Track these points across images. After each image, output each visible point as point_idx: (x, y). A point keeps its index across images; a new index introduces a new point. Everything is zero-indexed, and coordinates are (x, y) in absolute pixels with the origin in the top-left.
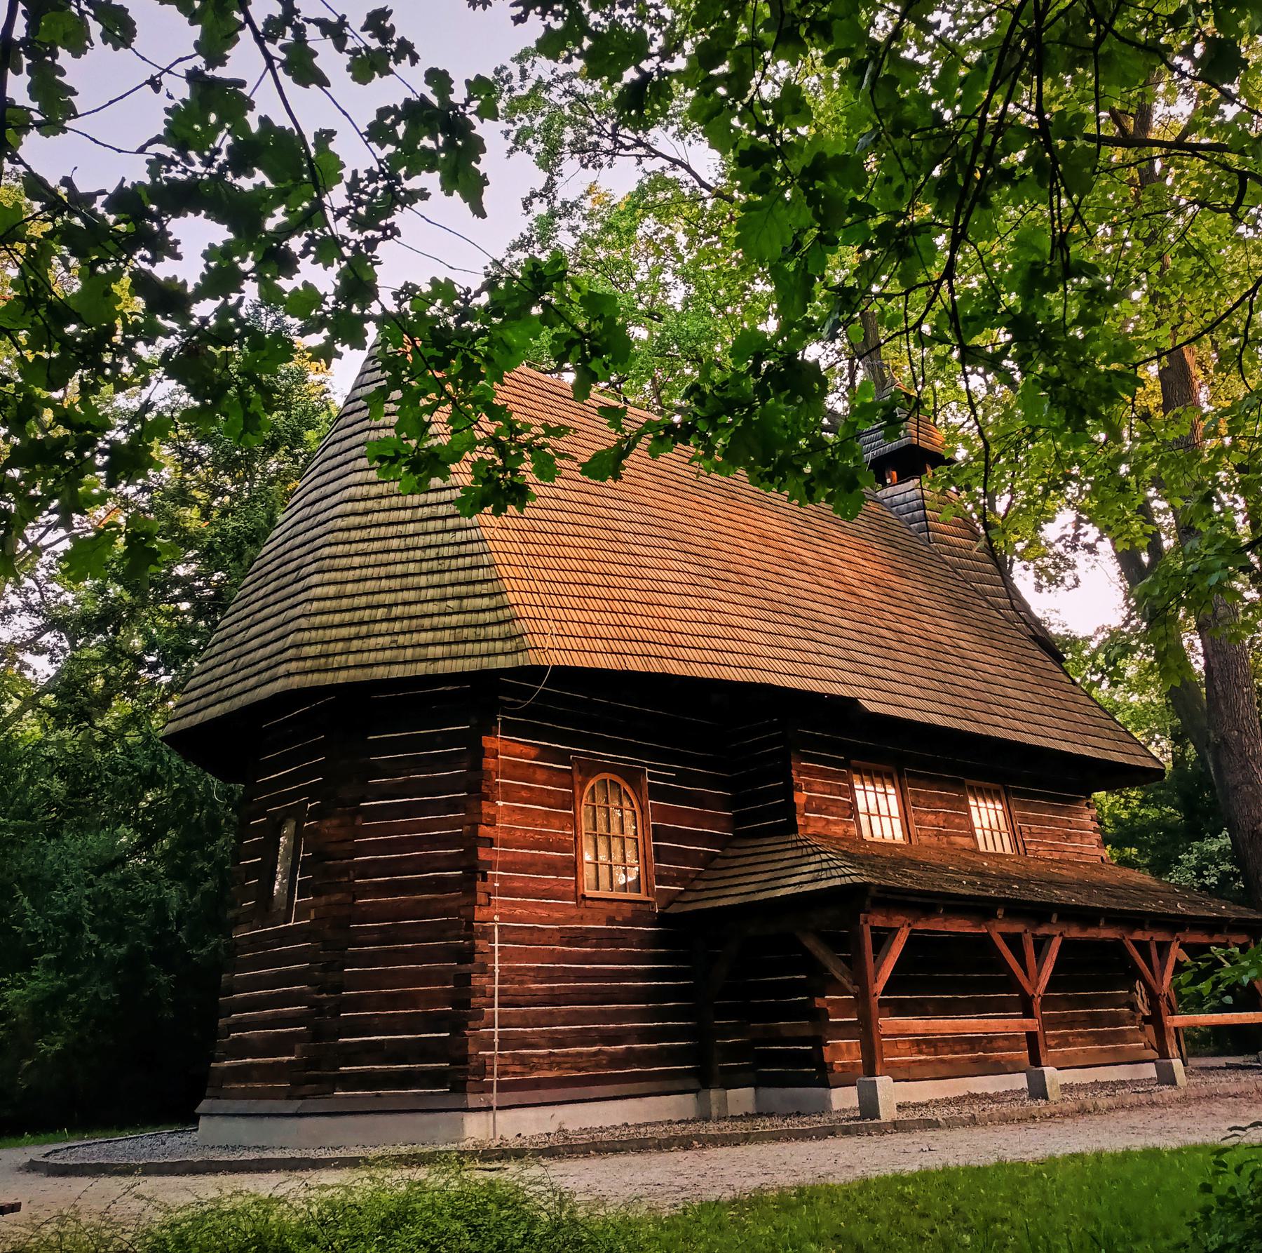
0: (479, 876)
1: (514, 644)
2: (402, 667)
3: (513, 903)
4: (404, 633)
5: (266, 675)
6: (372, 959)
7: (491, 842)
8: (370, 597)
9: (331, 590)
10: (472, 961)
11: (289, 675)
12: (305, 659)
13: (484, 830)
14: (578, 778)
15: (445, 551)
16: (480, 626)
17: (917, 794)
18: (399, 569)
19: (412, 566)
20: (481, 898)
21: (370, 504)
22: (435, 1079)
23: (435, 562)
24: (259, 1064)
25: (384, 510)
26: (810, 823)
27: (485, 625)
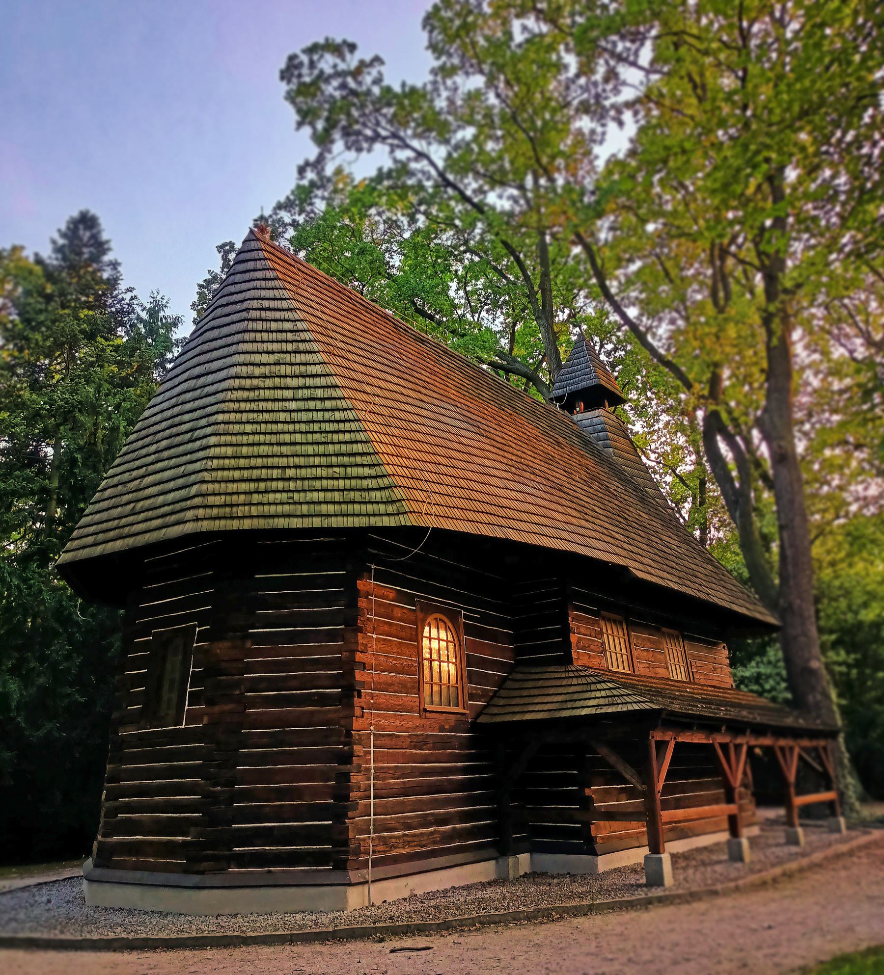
0: (356, 693)
1: (395, 507)
2: (300, 520)
3: (379, 715)
4: (299, 491)
5: (173, 518)
6: (263, 759)
7: (364, 666)
8: (265, 460)
9: (229, 451)
10: (350, 763)
11: (197, 519)
12: (211, 507)
13: (359, 656)
14: (420, 615)
15: (327, 427)
16: (364, 490)
17: (637, 638)
18: (288, 438)
19: (299, 436)
20: (357, 711)
21: (255, 382)
22: (319, 858)
23: (319, 435)
24: (151, 843)
25: (269, 388)
26: (580, 657)
27: (369, 490)
